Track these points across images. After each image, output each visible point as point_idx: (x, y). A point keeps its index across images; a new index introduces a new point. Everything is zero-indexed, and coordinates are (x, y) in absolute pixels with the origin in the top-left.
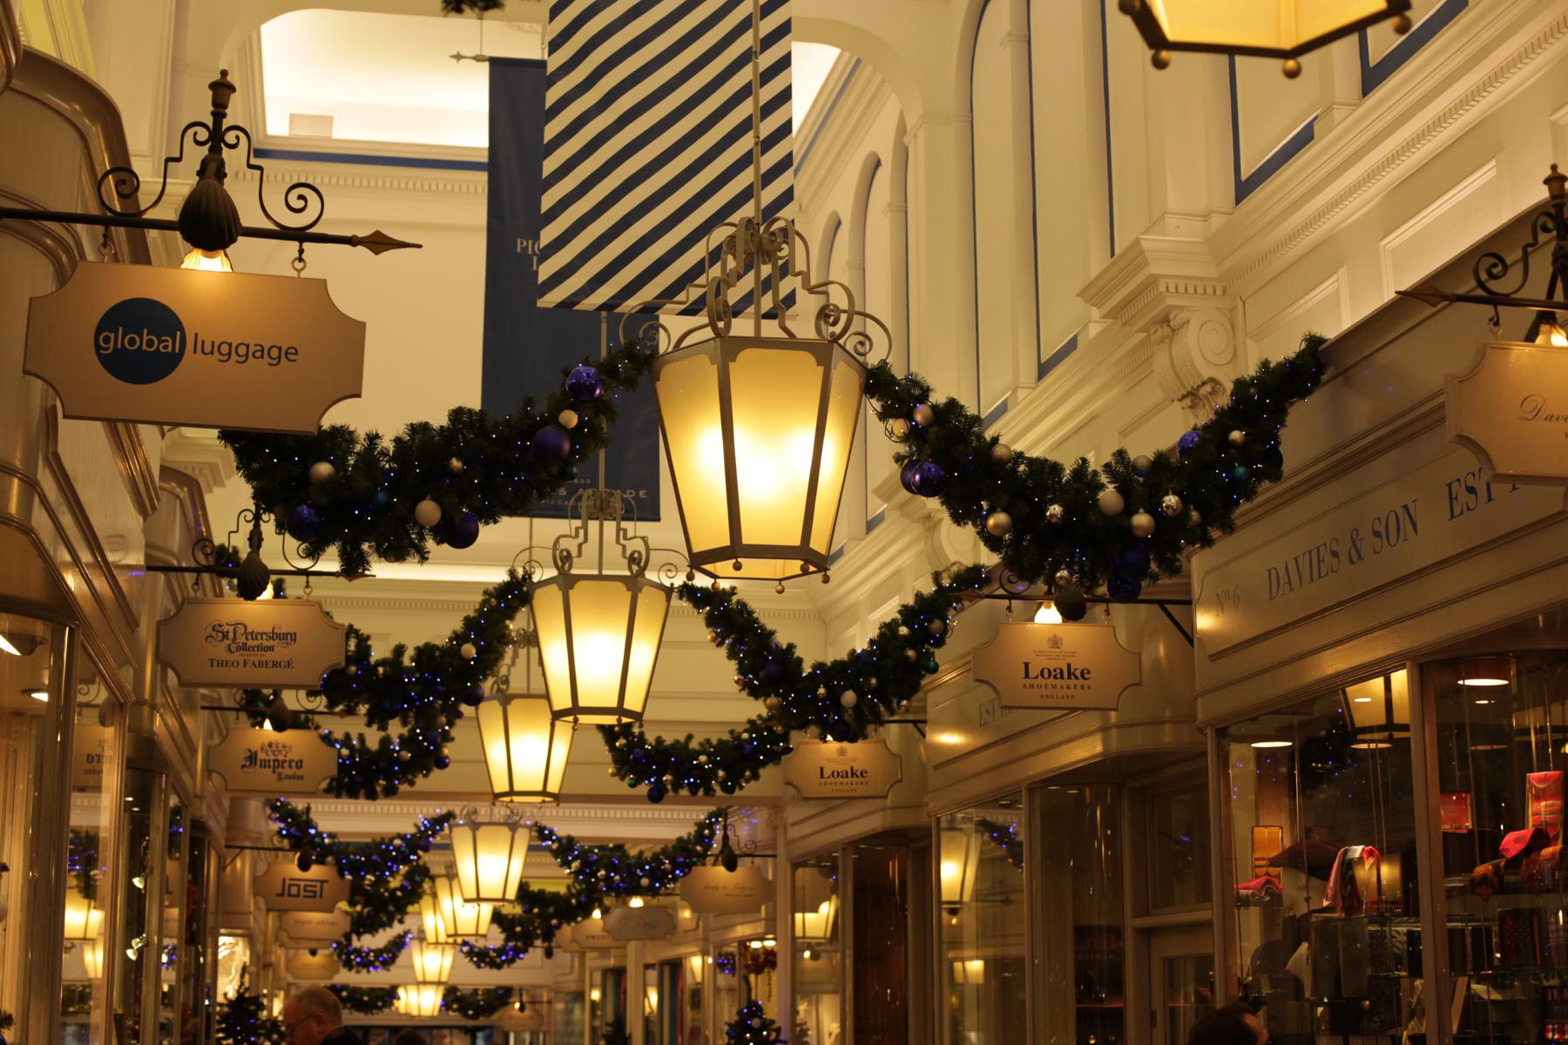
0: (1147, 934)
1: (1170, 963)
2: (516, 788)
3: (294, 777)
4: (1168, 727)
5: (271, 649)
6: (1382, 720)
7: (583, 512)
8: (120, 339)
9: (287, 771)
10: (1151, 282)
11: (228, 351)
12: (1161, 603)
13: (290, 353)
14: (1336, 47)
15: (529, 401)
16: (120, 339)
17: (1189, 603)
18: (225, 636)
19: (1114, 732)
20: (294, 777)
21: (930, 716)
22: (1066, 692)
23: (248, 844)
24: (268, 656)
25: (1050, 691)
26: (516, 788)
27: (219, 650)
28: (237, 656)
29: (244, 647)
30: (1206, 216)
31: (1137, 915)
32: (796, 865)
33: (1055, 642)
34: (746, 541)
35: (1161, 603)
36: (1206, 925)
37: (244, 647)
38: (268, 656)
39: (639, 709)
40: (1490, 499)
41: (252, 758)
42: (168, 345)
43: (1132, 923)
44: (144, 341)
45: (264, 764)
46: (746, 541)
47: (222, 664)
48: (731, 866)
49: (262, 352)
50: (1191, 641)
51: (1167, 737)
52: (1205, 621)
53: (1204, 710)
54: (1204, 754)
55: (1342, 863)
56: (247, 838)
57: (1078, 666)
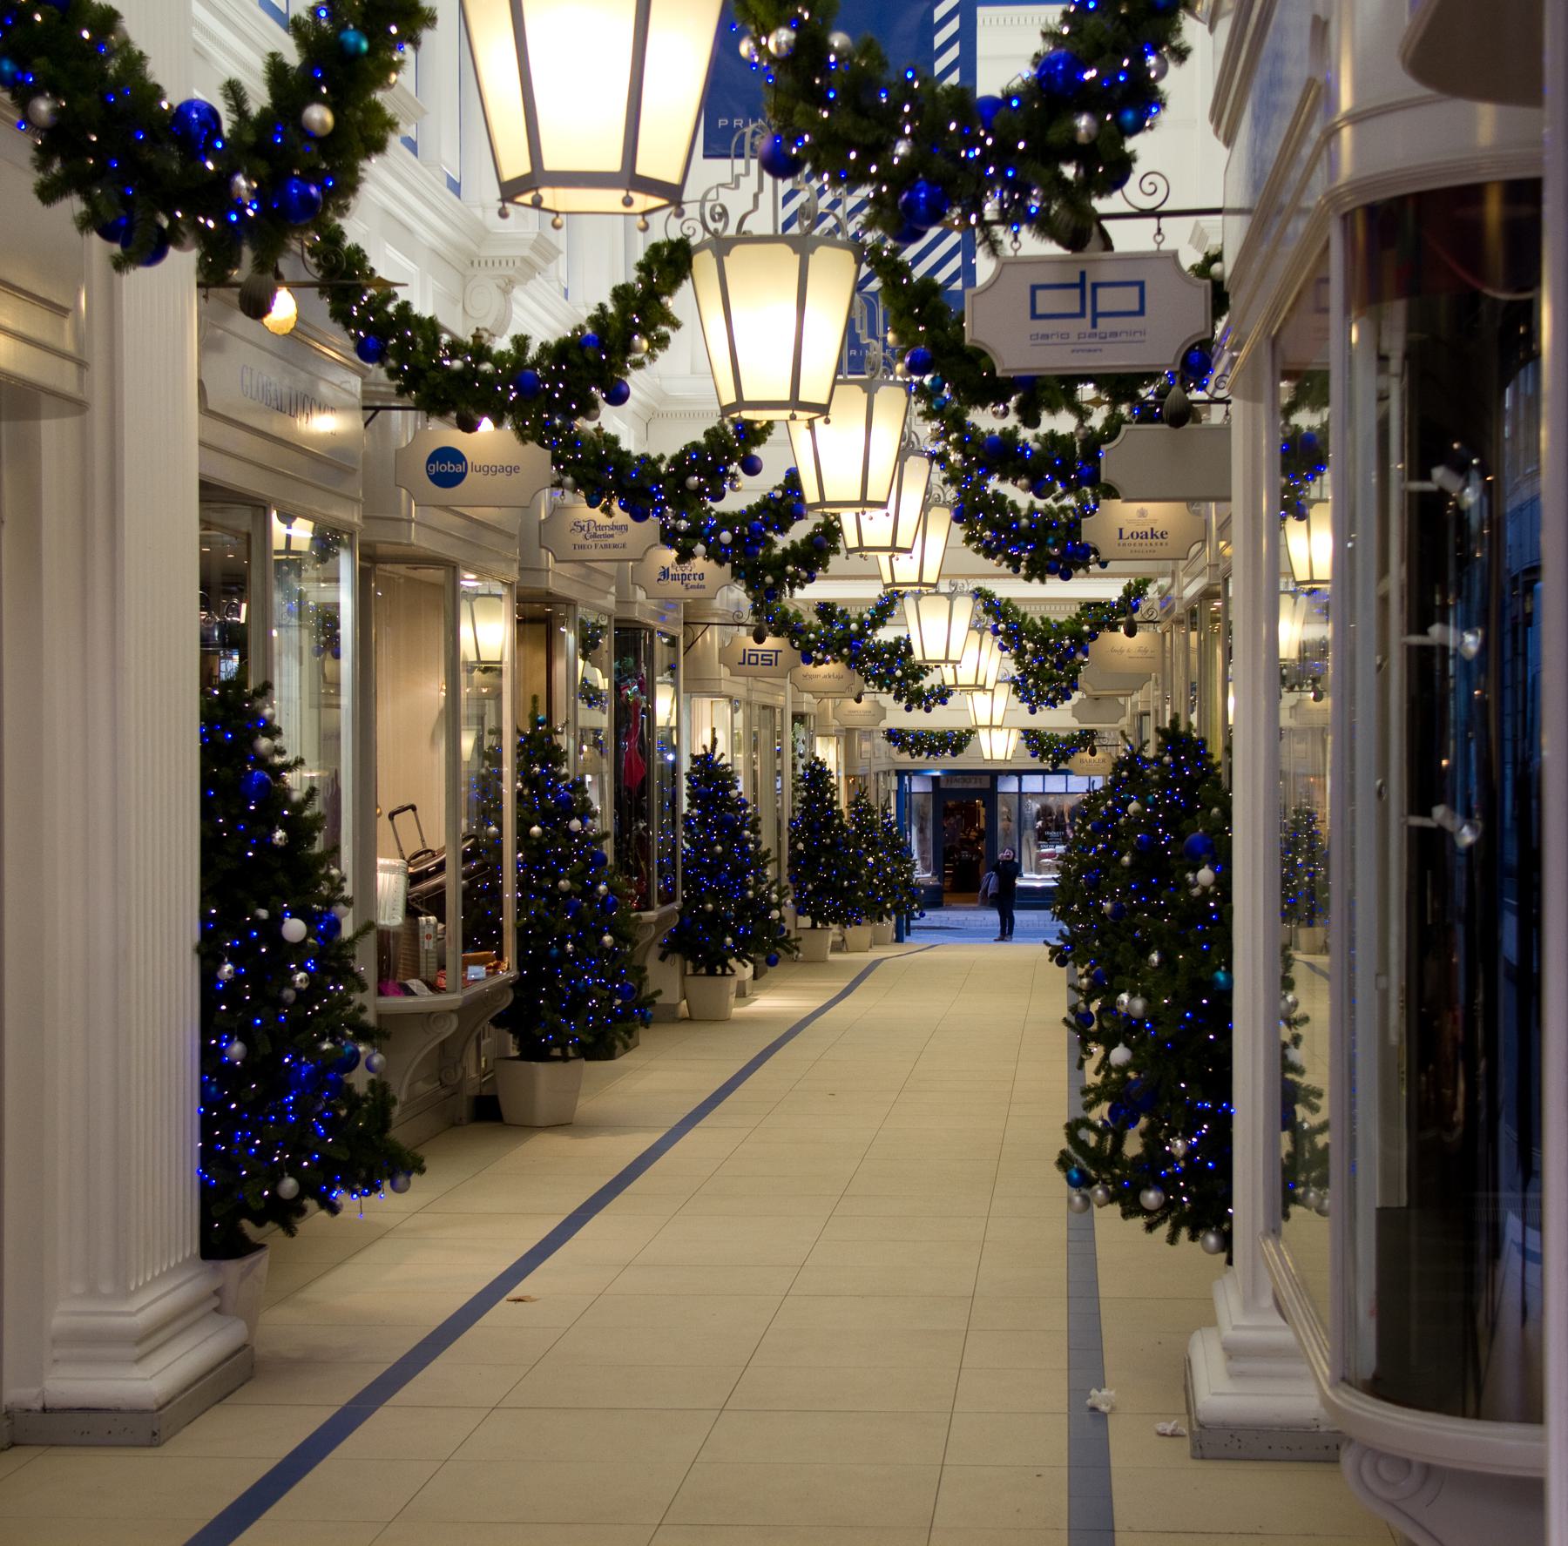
2: (828, 498)
3: (698, 587)
8: (437, 467)
9: (692, 582)
11: (487, 470)
13: (516, 469)
14: (1048, 311)
15: (827, 422)
16: (437, 467)
18: (582, 528)
20: (698, 587)
23: (716, 620)
24: (610, 541)
26: (828, 498)
27: (579, 538)
28: (590, 542)
29: (595, 536)
34: (801, 398)
37: (595, 536)
38: (610, 541)
39: (673, 177)
42: (459, 469)
44: (449, 467)
45: (675, 577)
46: (801, 398)
47: (582, 547)
49: (503, 469)
55: (1468, 599)
56: (714, 615)
57: (1158, 529)
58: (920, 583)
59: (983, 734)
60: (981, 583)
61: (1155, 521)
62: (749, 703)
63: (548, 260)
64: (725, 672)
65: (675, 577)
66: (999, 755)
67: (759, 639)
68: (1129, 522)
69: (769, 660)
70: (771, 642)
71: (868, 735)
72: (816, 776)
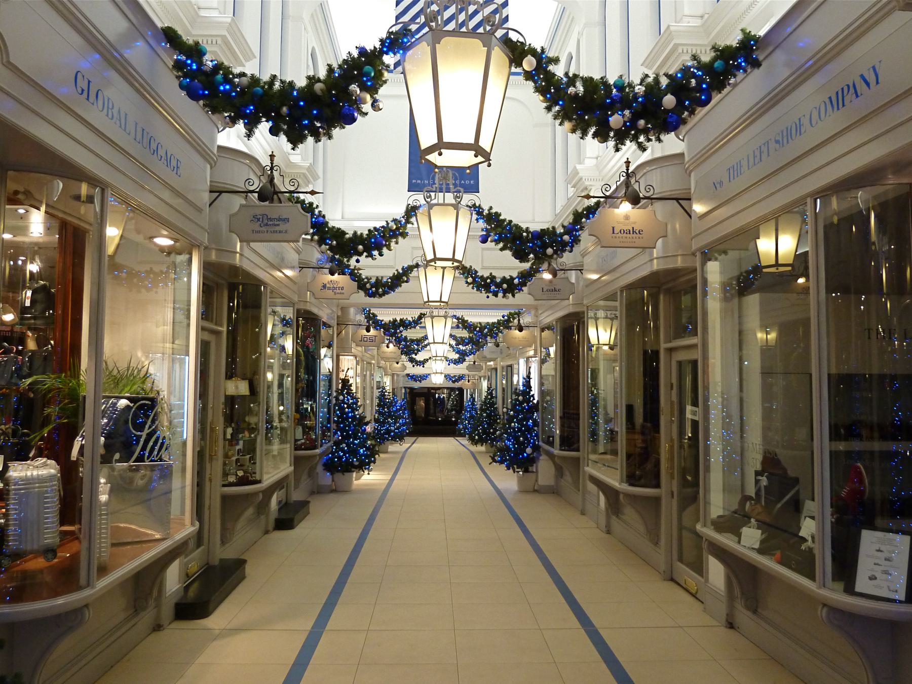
0: (670, 350)
1: (680, 363)
4: (679, 258)
5: (278, 225)
6: (774, 263)
7: (444, 190)
9: (338, 291)
10: (676, 46)
12: (677, 200)
17: (690, 199)
18: (259, 220)
19: (655, 261)
21: (585, 268)
22: (631, 240)
25: (624, 240)
28: (264, 229)
30: (702, 17)
31: (665, 342)
32: (543, 330)
33: (627, 217)
35: (677, 200)
36: (694, 346)
37: (267, 225)
38: (277, 228)
40: (877, 83)
41: (324, 286)
43: (663, 346)
45: (329, 289)
47: (259, 232)
48: (521, 330)
50: (690, 217)
51: (679, 263)
52: (699, 208)
53: (696, 245)
54: (696, 270)
57: (637, 228)
58: (441, 301)
59: (433, 376)
60: (459, 313)
61: (635, 223)
62: (363, 361)
63: (247, 60)
64: (353, 345)
65: (329, 289)
66: (438, 382)
67: (368, 331)
68: (619, 223)
69: (372, 340)
70: (373, 332)
71: (398, 375)
72: (381, 387)
